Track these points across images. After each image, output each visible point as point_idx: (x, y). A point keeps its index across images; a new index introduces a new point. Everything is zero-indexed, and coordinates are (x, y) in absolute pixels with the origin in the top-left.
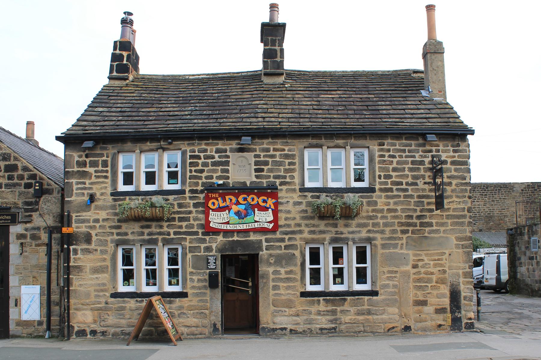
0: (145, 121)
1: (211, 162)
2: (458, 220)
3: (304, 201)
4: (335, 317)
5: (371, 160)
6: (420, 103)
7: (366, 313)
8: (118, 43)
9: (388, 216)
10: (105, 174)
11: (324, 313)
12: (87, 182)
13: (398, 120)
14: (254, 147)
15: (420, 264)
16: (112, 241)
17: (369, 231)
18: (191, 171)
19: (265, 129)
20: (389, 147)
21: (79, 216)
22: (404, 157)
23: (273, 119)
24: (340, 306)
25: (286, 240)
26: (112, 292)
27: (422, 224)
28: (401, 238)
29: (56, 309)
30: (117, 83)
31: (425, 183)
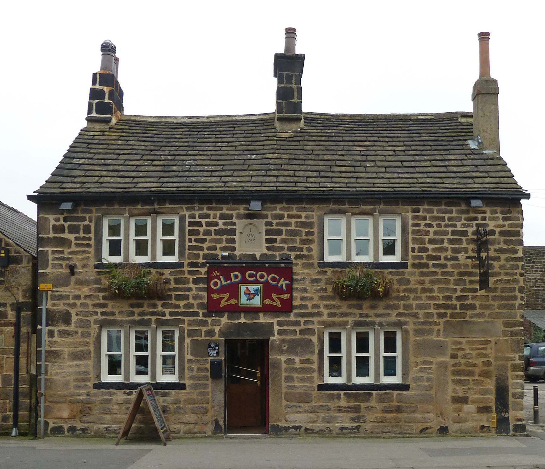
0: (134, 177)
1: (214, 229)
2: (506, 302)
3: (323, 278)
4: (358, 414)
5: (404, 230)
6: (466, 158)
7: (394, 411)
8: (98, 76)
9: (421, 297)
10: (87, 242)
11: (345, 409)
12: (66, 251)
13: (437, 180)
14: (265, 212)
15: (460, 353)
16: (96, 322)
17: (399, 315)
18: (190, 241)
19: (279, 192)
20: (425, 214)
21: (56, 291)
22: (443, 226)
23: (288, 179)
24: (364, 401)
25: (302, 324)
26: (95, 382)
27: (463, 307)
28: (438, 323)
29: (24, 401)
30: (97, 126)
31: (468, 258)
